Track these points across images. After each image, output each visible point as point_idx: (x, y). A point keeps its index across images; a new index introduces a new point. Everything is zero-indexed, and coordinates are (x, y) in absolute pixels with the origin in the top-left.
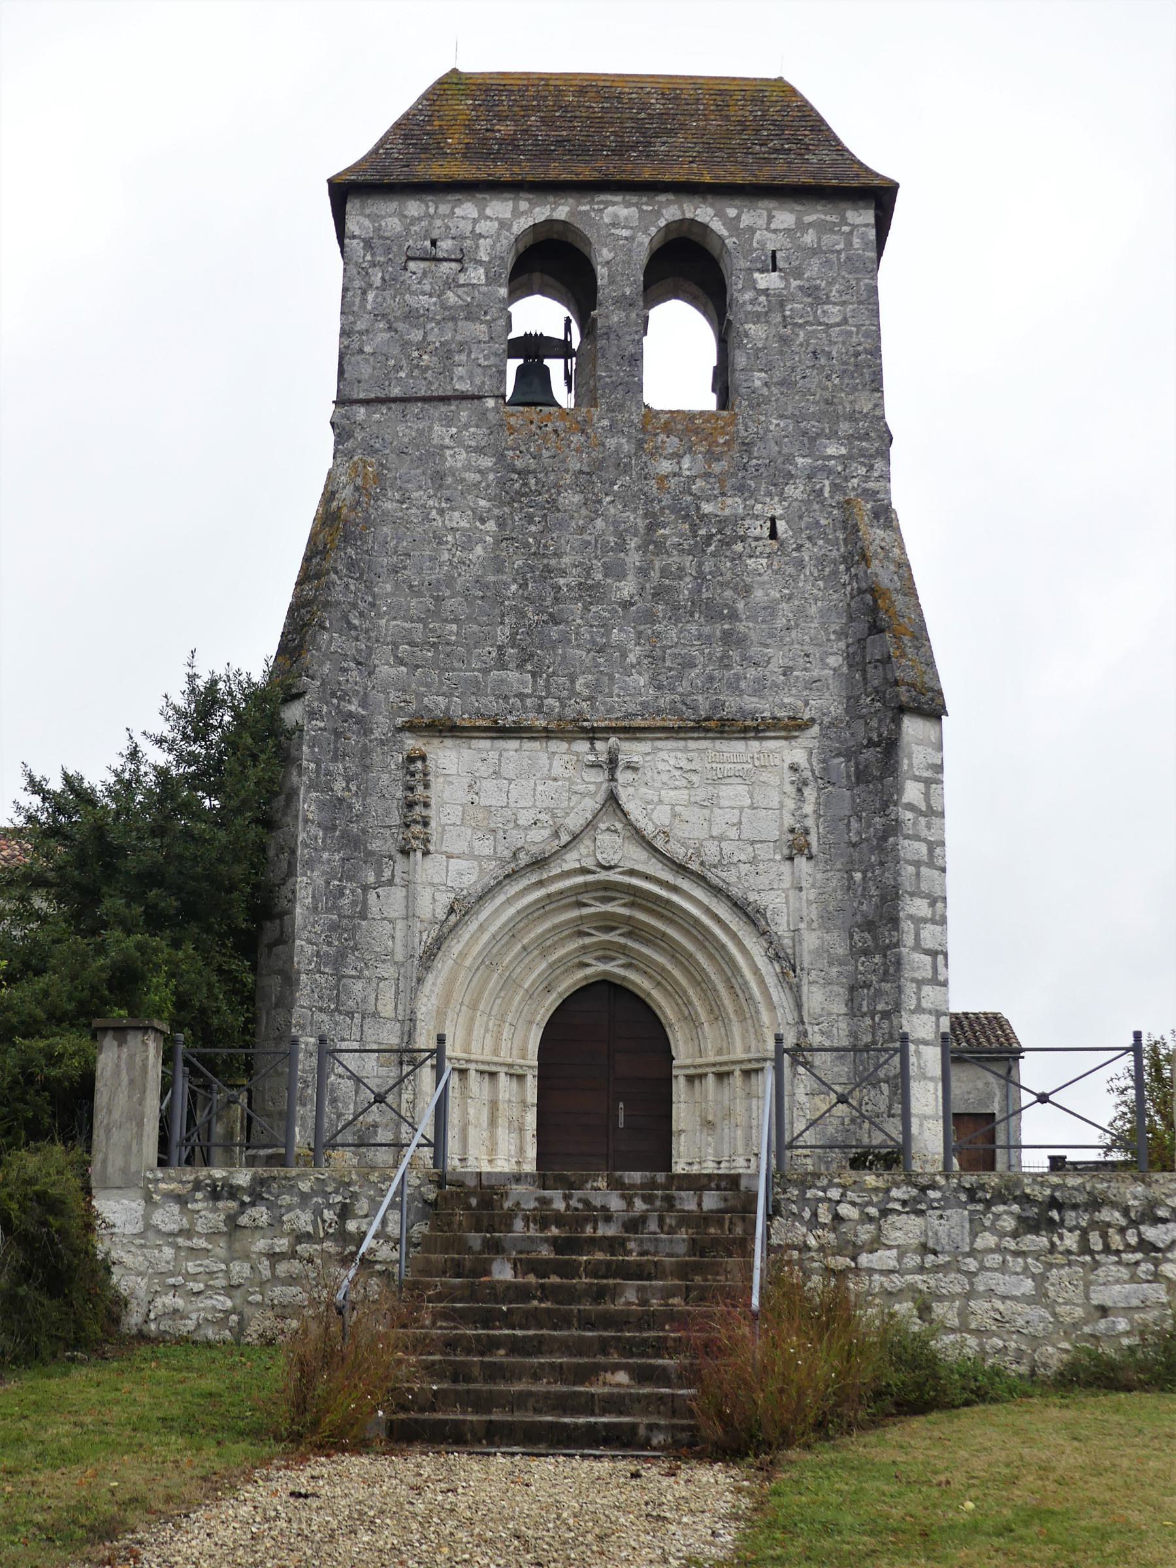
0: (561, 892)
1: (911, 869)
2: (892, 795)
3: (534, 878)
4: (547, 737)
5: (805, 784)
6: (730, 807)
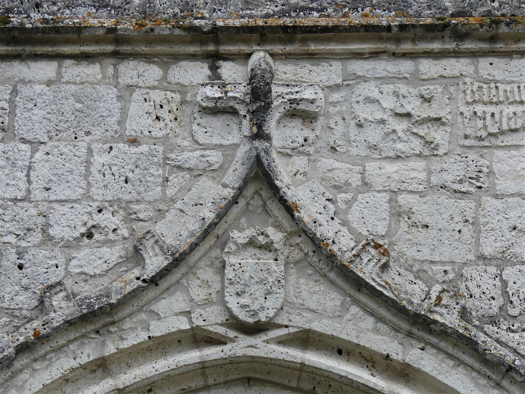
4: (116, 55)
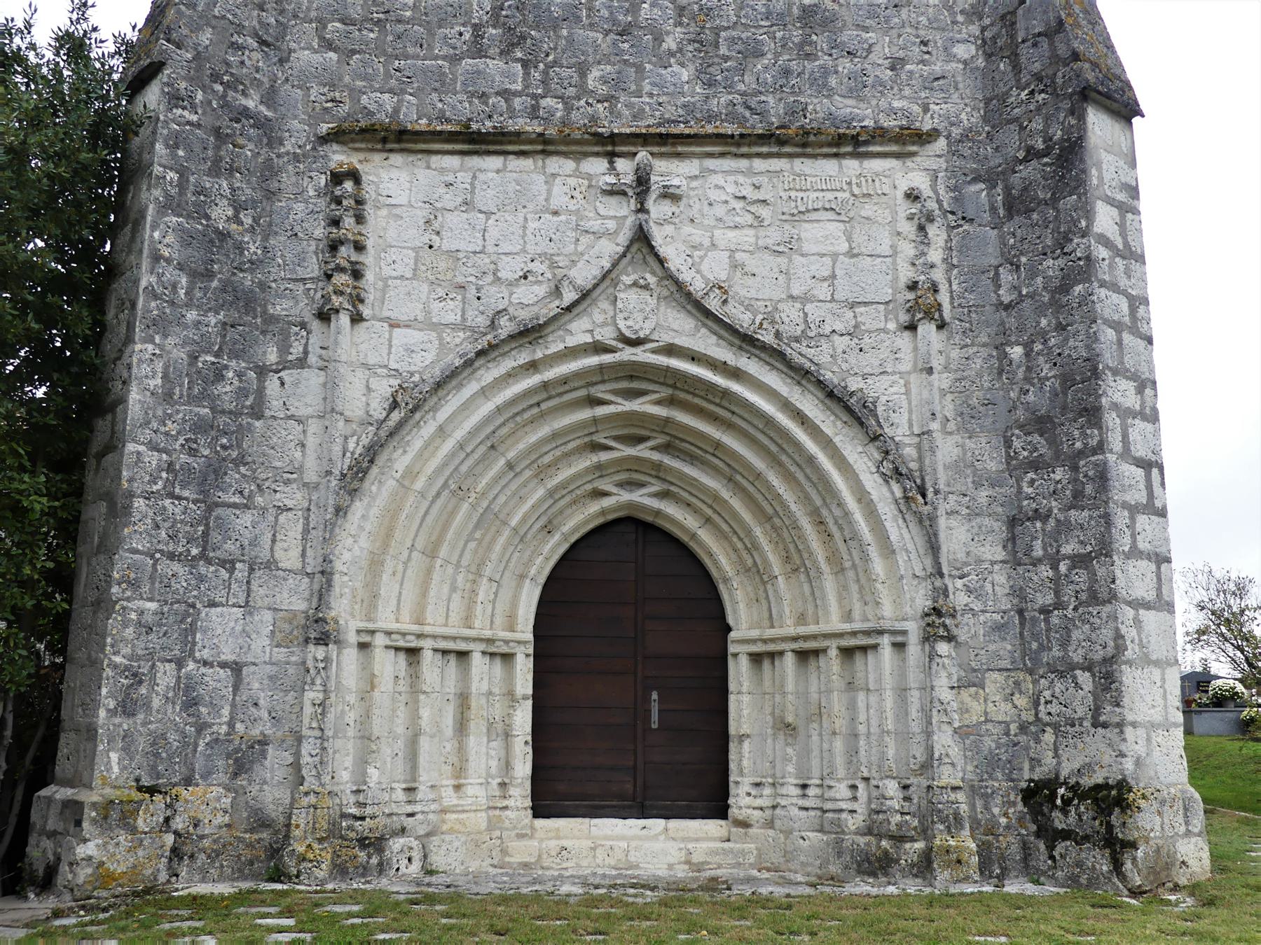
0: (564, 380)
1: (1110, 334)
2: (1075, 222)
3: (523, 357)
4: (543, 152)
5: (931, 219)
6: (823, 256)
